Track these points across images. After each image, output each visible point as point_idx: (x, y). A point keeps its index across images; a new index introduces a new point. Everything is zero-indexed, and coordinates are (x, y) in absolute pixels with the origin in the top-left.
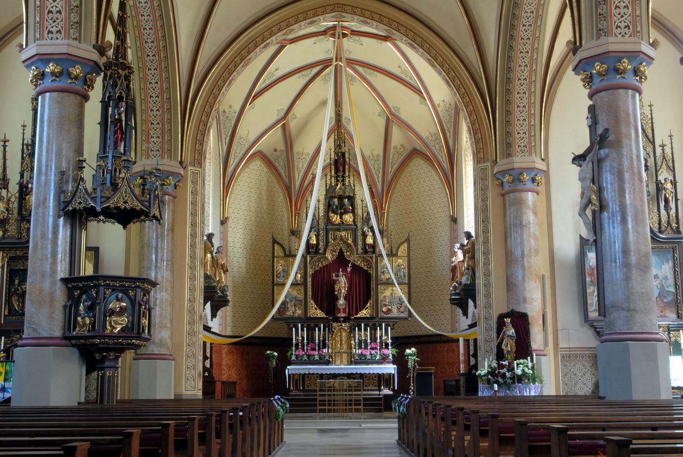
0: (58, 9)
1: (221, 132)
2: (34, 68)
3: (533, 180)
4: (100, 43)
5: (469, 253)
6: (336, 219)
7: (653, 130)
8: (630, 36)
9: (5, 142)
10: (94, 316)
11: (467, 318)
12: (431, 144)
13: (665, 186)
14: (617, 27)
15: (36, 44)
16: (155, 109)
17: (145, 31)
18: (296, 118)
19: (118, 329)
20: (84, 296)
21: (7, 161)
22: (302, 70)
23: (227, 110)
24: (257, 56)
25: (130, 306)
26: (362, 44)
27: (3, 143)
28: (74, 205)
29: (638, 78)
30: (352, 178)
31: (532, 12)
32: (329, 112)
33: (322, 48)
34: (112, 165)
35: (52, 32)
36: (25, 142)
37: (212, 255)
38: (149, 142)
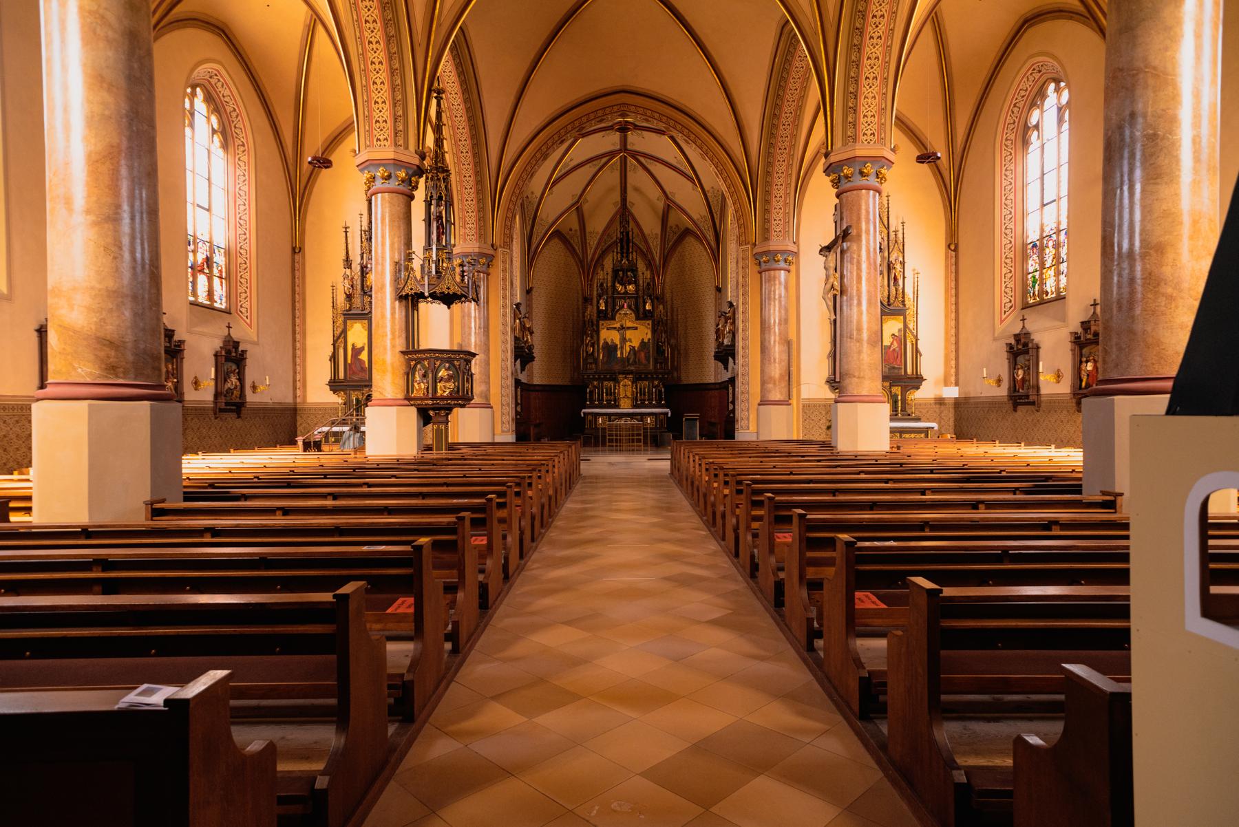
0: (384, 119)
2: (366, 172)
3: (786, 261)
4: (421, 148)
5: (730, 319)
6: (620, 288)
7: (888, 218)
8: (875, 142)
9: (346, 228)
10: (428, 382)
11: (727, 371)
12: (701, 225)
13: (895, 266)
14: (864, 134)
15: (367, 151)
18: (587, 202)
20: (419, 366)
22: (593, 161)
23: (529, 196)
24: (554, 151)
25: (456, 373)
27: (344, 230)
28: (407, 290)
29: (879, 180)
30: (634, 253)
31: (791, 113)
32: (617, 196)
33: (611, 141)
34: (436, 256)
35: (380, 140)
36: (363, 228)
37: (520, 321)
38: (465, 228)
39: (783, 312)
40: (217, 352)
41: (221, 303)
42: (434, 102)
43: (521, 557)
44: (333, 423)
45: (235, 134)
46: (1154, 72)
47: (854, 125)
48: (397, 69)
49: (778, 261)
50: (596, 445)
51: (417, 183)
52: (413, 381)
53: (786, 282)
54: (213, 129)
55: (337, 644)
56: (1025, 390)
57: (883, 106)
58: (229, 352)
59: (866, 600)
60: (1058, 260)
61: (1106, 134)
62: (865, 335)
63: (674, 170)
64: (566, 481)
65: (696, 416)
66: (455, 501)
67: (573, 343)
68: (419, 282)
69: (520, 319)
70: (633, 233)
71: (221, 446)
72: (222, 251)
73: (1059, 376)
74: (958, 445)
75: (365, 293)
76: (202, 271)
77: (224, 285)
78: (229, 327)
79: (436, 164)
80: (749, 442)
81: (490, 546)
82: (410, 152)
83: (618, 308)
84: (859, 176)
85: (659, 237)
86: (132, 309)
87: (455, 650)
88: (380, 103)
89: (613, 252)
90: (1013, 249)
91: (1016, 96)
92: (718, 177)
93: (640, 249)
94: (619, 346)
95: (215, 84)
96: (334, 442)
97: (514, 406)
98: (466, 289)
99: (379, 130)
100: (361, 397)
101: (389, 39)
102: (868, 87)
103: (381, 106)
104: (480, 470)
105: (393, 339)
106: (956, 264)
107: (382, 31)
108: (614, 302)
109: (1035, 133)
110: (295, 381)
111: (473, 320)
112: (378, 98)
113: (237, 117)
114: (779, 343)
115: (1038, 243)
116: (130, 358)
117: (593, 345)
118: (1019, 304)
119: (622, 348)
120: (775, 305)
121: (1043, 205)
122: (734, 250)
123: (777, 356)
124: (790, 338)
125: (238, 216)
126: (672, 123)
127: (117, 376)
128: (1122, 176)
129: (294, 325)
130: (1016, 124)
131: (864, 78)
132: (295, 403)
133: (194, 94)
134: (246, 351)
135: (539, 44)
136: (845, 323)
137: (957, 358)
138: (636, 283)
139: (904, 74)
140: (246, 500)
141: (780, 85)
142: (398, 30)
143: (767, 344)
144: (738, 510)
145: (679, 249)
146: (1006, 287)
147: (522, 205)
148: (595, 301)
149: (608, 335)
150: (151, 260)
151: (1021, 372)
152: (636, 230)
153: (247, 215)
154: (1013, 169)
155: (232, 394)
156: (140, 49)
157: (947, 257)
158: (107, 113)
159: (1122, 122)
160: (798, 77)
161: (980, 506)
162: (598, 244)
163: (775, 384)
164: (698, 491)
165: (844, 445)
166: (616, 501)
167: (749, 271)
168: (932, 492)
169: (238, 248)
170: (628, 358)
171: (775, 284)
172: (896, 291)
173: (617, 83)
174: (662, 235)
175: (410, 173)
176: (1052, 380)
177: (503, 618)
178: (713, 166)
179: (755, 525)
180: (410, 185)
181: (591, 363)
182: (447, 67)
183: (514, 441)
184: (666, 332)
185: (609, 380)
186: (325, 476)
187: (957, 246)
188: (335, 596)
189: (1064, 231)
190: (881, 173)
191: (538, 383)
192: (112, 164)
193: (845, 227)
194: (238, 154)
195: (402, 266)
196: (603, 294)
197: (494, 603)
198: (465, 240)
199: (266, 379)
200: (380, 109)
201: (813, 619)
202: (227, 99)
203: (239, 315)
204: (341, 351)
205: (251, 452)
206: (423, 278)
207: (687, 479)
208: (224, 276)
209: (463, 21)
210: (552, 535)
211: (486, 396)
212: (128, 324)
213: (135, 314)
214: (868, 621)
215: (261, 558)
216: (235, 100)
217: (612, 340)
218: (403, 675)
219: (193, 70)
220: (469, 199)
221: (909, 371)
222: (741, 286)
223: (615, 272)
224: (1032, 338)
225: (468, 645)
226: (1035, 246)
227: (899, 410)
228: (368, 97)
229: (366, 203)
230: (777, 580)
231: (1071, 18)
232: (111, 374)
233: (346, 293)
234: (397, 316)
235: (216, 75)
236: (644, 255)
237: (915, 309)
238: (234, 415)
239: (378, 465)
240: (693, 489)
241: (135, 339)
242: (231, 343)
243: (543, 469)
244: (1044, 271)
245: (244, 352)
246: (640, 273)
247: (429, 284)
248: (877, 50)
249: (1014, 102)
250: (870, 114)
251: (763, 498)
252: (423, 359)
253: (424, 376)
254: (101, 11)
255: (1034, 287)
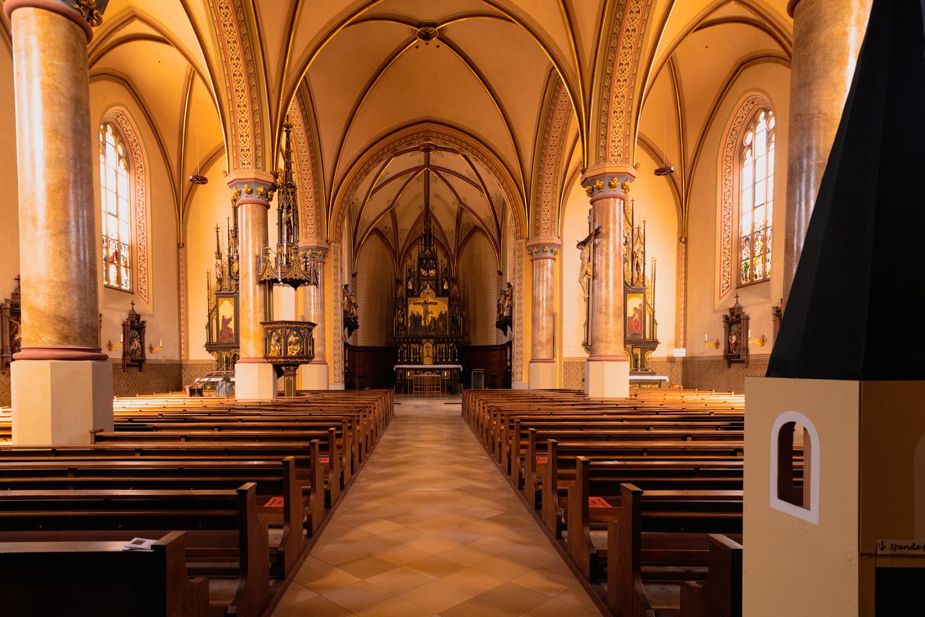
0: (247, 148)
1: (351, 216)
3: (552, 251)
4: (274, 170)
5: (509, 296)
6: (424, 272)
7: (633, 218)
8: (621, 162)
9: (217, 229)
10: (281, 345)
11: (506, 336)
13: (638, 255)
16: (309, 206)
17: (306, 181)
19: (295, 353)
20: (274, 333)
21: (220, 242)
23: (355, 202)
24: (374, 168)
25: (301, 339)
26: (443, 156)
27: (216, 230)
28: (265, 277)
29: (624, 190)
30: (435, 245)
31: (557, 137)
32: (421, 202)
33: (417, 159)
35: (244, 164)
36: (230, 229)
37: (348, 297)
38: (307, 228)
39: (549, 291)
40: (124, 322)
41: (126, 286)
42: (284, 134)
43: (352, 473)
44: (210, 376)
45: (135, 159)
46: (824, 117)
47: (605, 148)
48: (257, 110)
49: (546, 252)
50: (405, 392)
51: (272, 196)
52: (270, 345)
53: (552, 267)
54: (119, 155)
55: (239, 522)
56: (737, 352)
57: (628, 133)
58: (133, 322)
59: (597, 502)
60: (765, 250)
61: (789, 162)
62: (611, 310)
63: (466, 181)
64: (383, 418)
65: (483, 371)
66: (306, 432)
67: (388, 314)
68: (273, 270)
69: (347, 297)
70: (434, 230)
71: (128, 392)
72: (127, 247)
73: (763, 341)
74: (683, 394)
75: (231, 277)
76: (112, 262)
77: (128, 273)
78: (133, 304)
79: (286, 182)
80: (522, 391)
81: (331, 464)
82: (267, 173)
83: (422, 288)
84: (608, 188)
85: (454, 232)
86: (78, 295)
87: (309, 535)
88: (245, 136)
89: (419, 244)
90: (730, 241)
91: (734, 122)
92: (500, 187)
93: (440, 242)
94: (423, 317)
95: (121, 122)
96: (210, 389)
97: (343, 363)
98: (309, 276)
99: (243, 157)
100: (229, 356)
101: (251, 88)
102: (616, 119)
103: (245, 138)
104: (321, 410)
105: (255, 313)
106: (686, 253)
107: (246, 82)
108: (419, 283)
109: (749, 151)
110: (180, 344)
111: (312, 298)
112: (243, 132)
113: (137, 146)
114: (546, 315)
115: (750, 237)
116: (78, 330)
117: (403, 316)
118: (734, 285)
119: (425, 318)
120: (543, 285)
121: (754, 208)
122: (512, 243)
123: (544, 325)
124: (554, 311)
125: (138, 221)
126: (464, 145)
127: (69, 343)
128: (800, 194)
129: (179, 302)
130: (734, 144)
131: (613, 112)
132: (181, 360)
133: (105, 130)
134: (145, 322)
135: (362, 86)
136: (596, 300)
137: (685, 327)
138: (436, 269)
139: (644, 108)
140: (157, 431)
141: (549, 116)
142: (258, 81)
143: (537, 316)
144: (510, 441)
145: (469, 242)
146: (724, 271)
147: (349, 209)
148: (404, 282)
149: (415, 308)
150: (90, 260)
151: (734, 338)
152: (436, 228)
153: (145, 220)
154: (731, 179)
155: (136, 353)
156: (82, 110)
157: (678, 249)
158: (60, 156)
159: (801, 154)
160: (562, 109)
161: (688, 438)
162: (408, 237)
163: (542, 346)
164: (482, 427)
165: (595, 393)
166: (420, 435)
167: (523, 260)
168: (655, 428)
169: (138, 245)
170: (430, 327)
171: (543, 270)
172: (638, 274)
173: (423, 115)
174: (456, 230)
175: (267, 188)
176: (758, 344)
177: (341, 514)
178: (496, 178)
179: (523, 451)
180: (267, 198)
181: (401, 330)
182: (294, 109)
183: (344, 389)
184: (459, 306)
185: (415, 343)
186: (210, 414)
187: (686, 239)
188: (237, 492)
189: (770, 228)
190: (625, 185)
191: (361, 345)
192: (64, 193)
193: (597, 227)
194: (138, 174)
195: (262, 259)
196: (411, 277)
197: (334, 504)
198: (306, 237)
199: (159, 342)
200: (245, 140)
201: (561, 516)
202: (129, 133)
203: (139, 294)
204: (214, 322)
205: (150, 397)
206: (277, 268)
207: (474, 419)
208: (128, 266)
209: (307, 72)
210: (374, 458)
211: (323, 355)
212: (75, 306)
213: (80, 299)
214: (600, 517)
215: (179, 469)
216: (135, 134)
217: (418, 312)
218: (277, 548)
219: (104, 113)
220: (309, 206)
221: (647, 336)
222: (517, 271)
223: (420, 260)
224: (743, 311)
225: (318, 532)
226: (747, 239)
227: (638, 366)
228: (235, 132)
229: (231, 211)
230: (537, 490)
231: (777, 62)
232: (65, 341)
233: (218, 278)
234: (258, 296)
235: (121, 115)
236: (442, 247)
237: (653, 289)
238: (137, 369)
239: (246, 407)
240: (478, 425)
241: (81, 316)
242: (135, 316)
243: (367, 410)
244: (754, 259)
245: (144, 322)
246: (439, 261)
247: (281, 272)
248: (623, 90)
249: (733, 127)
250: (617, 139)
251: (547, 443)
252: (277, 328)
253: (278, 341)
254: (56, 84)
255: (746, 271)
